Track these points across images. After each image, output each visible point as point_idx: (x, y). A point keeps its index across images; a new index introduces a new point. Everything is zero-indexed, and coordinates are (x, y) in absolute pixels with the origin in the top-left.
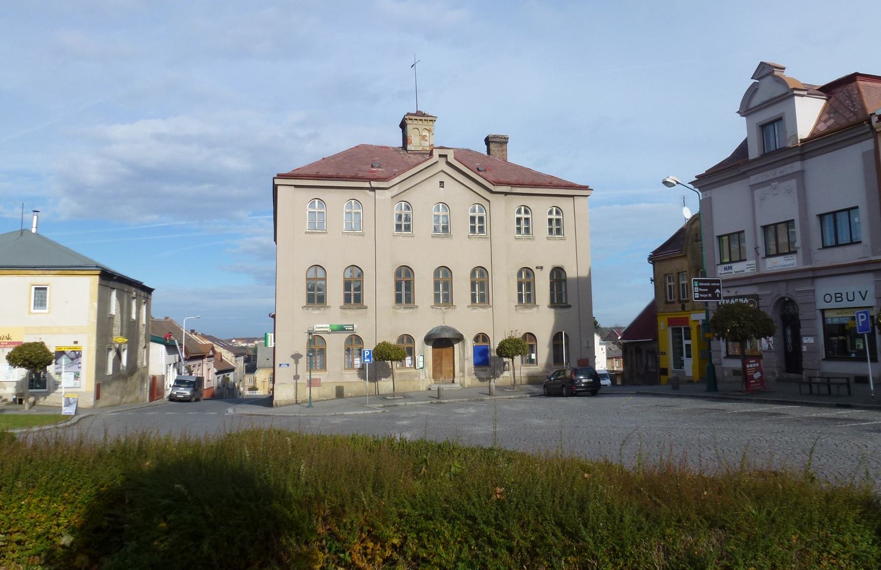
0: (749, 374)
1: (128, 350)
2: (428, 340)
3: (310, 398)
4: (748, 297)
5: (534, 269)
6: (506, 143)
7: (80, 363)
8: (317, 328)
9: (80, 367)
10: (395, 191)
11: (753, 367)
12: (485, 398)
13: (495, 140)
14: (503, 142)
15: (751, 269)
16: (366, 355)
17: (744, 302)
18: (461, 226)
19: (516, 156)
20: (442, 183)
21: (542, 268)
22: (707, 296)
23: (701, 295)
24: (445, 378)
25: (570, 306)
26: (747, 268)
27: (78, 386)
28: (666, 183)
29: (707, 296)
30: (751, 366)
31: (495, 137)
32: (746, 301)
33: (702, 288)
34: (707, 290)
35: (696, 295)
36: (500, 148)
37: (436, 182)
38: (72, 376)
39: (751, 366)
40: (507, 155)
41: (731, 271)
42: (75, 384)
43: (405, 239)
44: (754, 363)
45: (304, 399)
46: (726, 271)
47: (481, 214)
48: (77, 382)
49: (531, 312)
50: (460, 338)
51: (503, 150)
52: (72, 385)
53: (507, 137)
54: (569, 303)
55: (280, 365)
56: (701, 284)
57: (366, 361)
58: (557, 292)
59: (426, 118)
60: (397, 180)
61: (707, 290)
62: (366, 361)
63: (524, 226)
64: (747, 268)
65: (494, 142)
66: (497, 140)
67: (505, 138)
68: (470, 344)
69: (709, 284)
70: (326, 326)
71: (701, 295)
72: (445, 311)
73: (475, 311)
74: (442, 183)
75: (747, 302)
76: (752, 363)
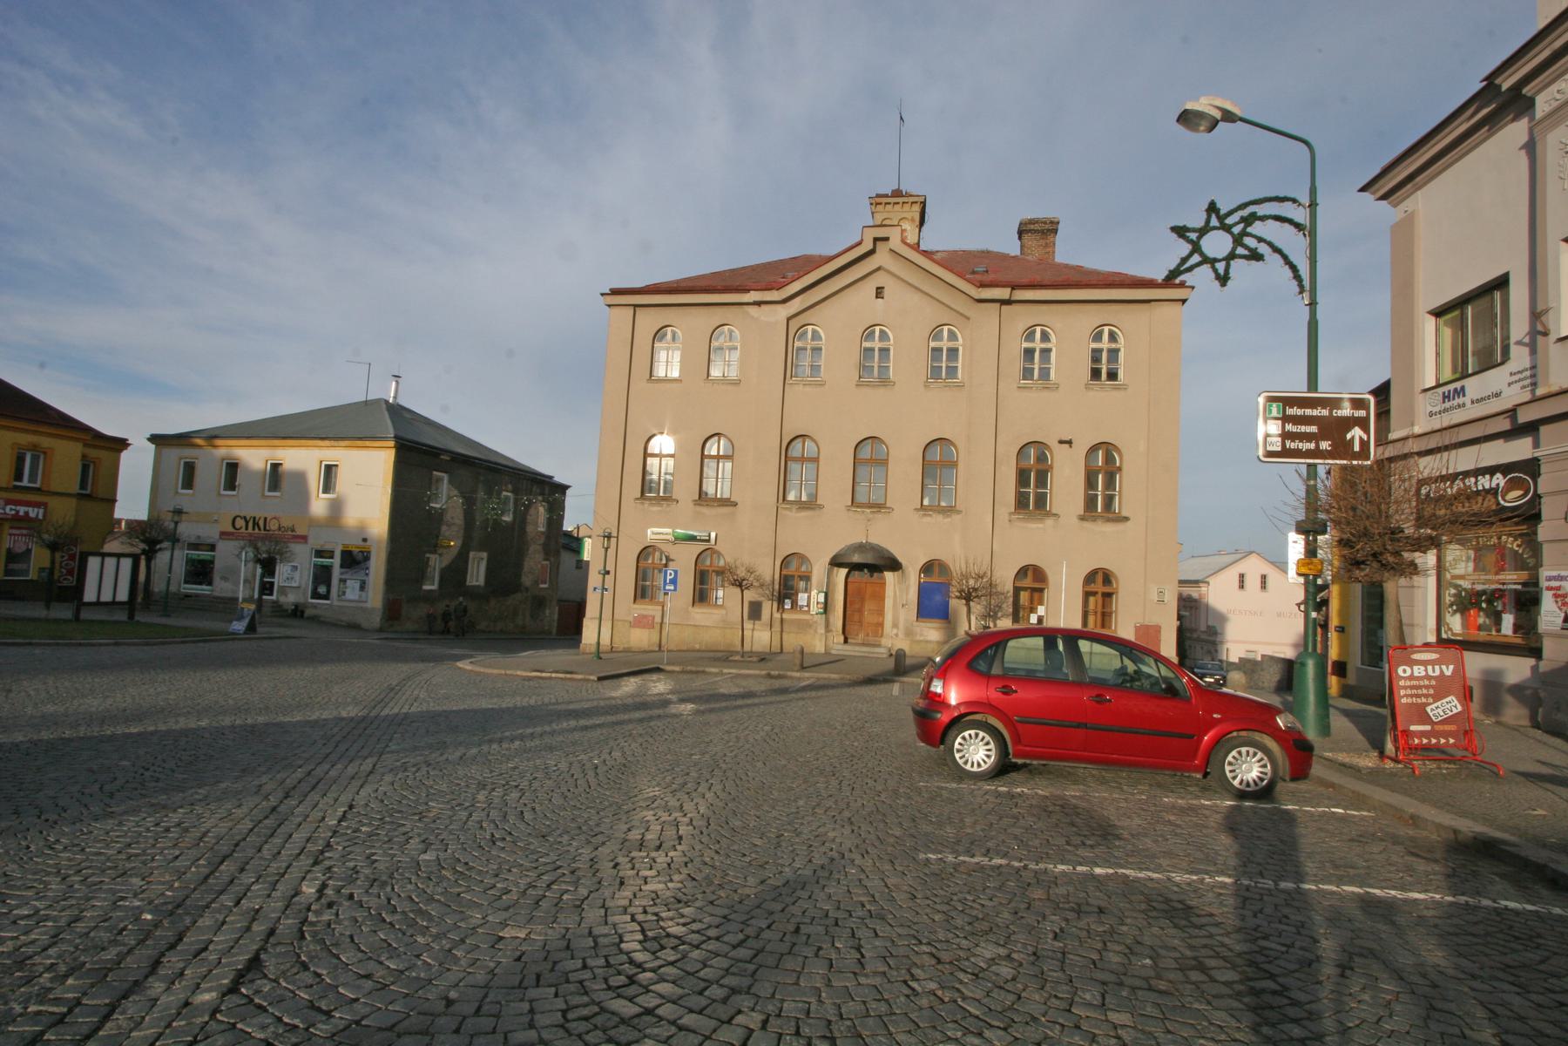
0: (1404, 700)
1: (488, 561)
2: (836, 563)
3: (598, 643)
4: (1505, 469)
5: (1053, 444)
6: (1055, 231)
7: (367, 568)
8: (653, 533)
9: (367, 574)
10: (796, 304)
11: (1428, 677)
12: (707, 669)
13: (1032, 227)
14: (1048, 230)
15: (1521, 384)
16: (669, 577)
17: (1493, 485)
18: (908, 362)
19: (1068, 251)
20: (879, 292)
21: (1070, 442)
22: (1312, 446)
23: (1290, 445)
24: (868, 635)
25: (1126, 519)
26: (1510, 384)
27: (364, 599)
28: (1187, 118)
29: (1312, 446)
30: (1419, 671)
31: (1032, 222)
32: (1499, 480)
33: (1294, 424)
34: (1313, 429)
35: (1271, 444)
36: (1042, 242)
37: (869, 287)
38: (357, 585)
39: (1419, 671)
40: (1054, 252)
41: (1460, 400)
42: (360, 596)
43: (808, 389)
44: (1433, 663)
45: (626, 646)
46: (1447, 405)
47: (951, 344)
48: (364, 594)
49: (1041, 526)
50: (894, 565)
51: (1047, 245)
52: (357, 598)
53: (1056, 220)
54: (1124, 514)
55: (595, 589)
56: (1293, 411)
57: (667, 587)
58: (1103, 491)
59: (905, 199)
60: (796, 286)
61: (1313, 429)
62: (667, 587)
63: (1034, 367)
64: (1510, 384)
65: (1030, 231)
66: (1037, 227)
67: (1052, 222)
68: (913, 578)
69: (1325, 412)
70: (666, 532)
71: (1290, 445)
72: (871, 516)
73: (928, 519)
74: (879, 292)
75: (1502, 485)
76: (1424, 663)
